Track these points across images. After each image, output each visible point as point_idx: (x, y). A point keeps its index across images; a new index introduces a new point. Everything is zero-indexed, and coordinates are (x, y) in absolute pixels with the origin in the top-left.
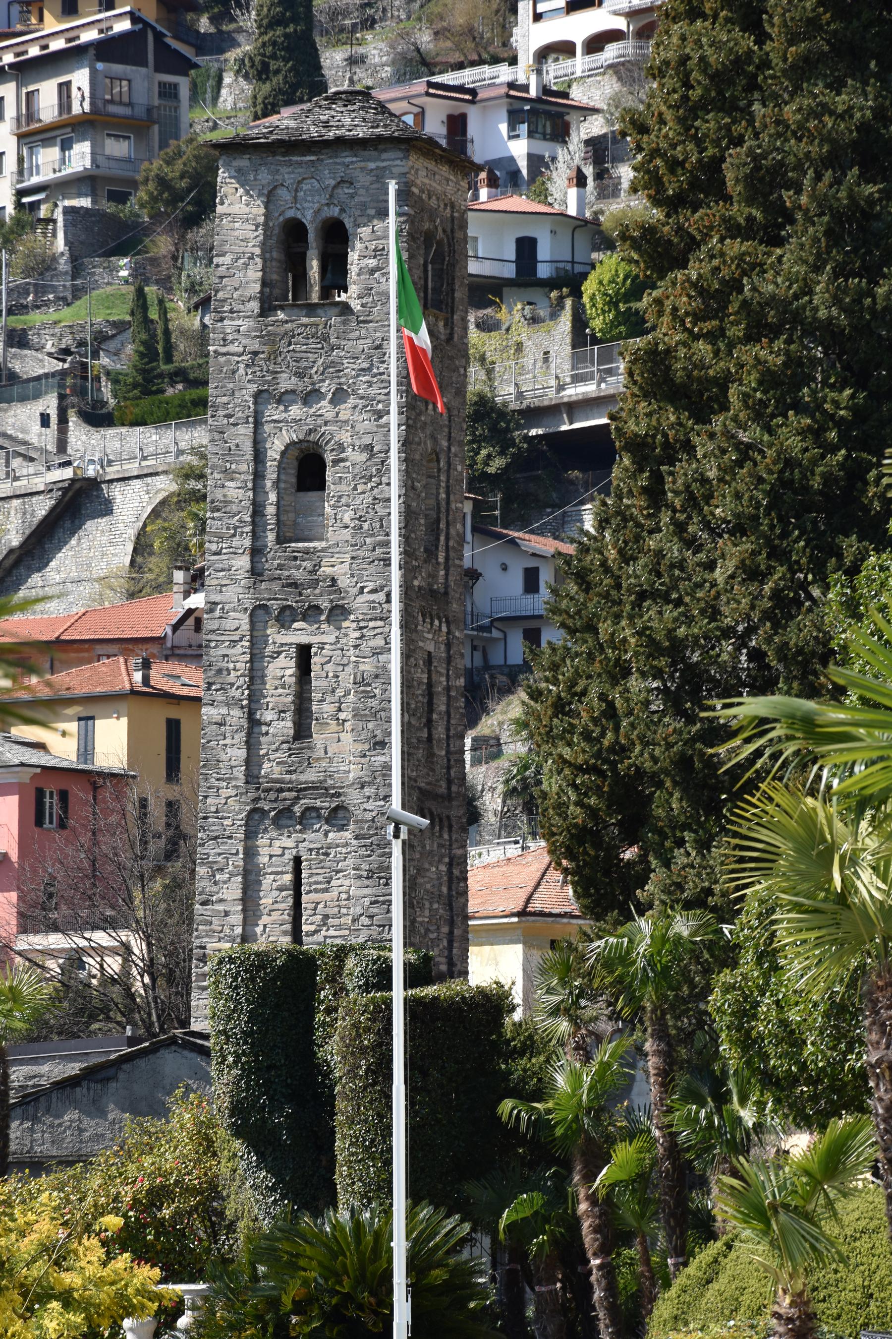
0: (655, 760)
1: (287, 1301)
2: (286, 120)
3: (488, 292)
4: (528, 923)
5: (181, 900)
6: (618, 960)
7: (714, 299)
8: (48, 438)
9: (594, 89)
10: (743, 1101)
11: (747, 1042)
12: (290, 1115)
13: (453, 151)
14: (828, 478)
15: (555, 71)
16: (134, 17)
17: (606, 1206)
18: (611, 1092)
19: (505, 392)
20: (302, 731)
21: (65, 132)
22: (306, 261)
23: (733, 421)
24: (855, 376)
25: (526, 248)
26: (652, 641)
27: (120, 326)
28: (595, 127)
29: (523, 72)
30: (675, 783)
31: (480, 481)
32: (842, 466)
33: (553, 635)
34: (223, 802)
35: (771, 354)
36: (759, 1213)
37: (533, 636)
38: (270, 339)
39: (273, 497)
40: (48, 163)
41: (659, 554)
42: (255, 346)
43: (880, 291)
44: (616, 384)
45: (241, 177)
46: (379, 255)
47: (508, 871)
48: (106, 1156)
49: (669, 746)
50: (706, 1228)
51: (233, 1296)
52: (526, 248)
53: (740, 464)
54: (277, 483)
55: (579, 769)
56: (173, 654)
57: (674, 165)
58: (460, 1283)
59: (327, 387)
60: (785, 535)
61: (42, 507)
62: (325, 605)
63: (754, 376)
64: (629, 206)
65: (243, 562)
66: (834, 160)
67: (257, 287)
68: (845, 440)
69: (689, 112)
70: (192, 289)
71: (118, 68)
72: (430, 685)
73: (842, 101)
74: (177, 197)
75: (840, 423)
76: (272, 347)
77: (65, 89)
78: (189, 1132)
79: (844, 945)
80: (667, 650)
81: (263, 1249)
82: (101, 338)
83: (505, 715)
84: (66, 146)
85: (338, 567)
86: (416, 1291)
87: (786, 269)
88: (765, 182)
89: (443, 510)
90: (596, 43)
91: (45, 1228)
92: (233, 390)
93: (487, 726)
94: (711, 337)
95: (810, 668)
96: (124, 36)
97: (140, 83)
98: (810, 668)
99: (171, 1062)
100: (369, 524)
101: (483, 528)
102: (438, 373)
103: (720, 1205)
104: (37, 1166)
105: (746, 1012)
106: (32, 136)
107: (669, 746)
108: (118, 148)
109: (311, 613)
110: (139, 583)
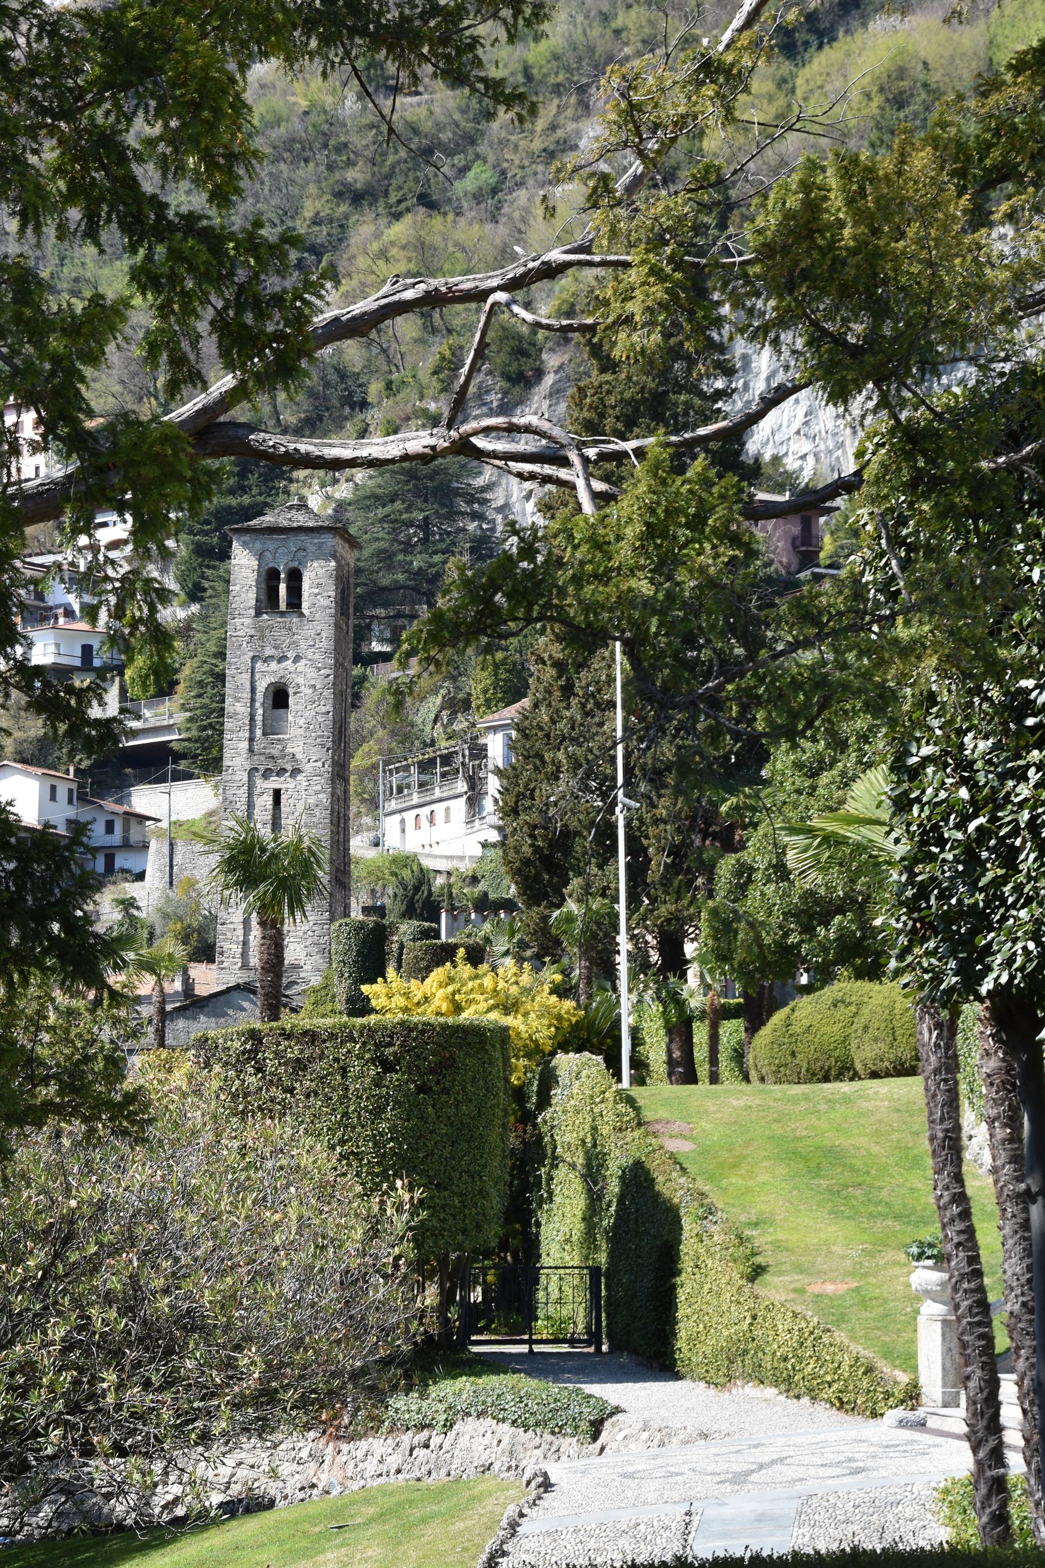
38: (260, 629)
39: (260, 711)
42: (252, 632)
45: (245, 545)
59: (291, 654)
62: (289, 768)
65: (245, 745)
76: (261, 634)
85: (297, 748)
109: (281, 772)
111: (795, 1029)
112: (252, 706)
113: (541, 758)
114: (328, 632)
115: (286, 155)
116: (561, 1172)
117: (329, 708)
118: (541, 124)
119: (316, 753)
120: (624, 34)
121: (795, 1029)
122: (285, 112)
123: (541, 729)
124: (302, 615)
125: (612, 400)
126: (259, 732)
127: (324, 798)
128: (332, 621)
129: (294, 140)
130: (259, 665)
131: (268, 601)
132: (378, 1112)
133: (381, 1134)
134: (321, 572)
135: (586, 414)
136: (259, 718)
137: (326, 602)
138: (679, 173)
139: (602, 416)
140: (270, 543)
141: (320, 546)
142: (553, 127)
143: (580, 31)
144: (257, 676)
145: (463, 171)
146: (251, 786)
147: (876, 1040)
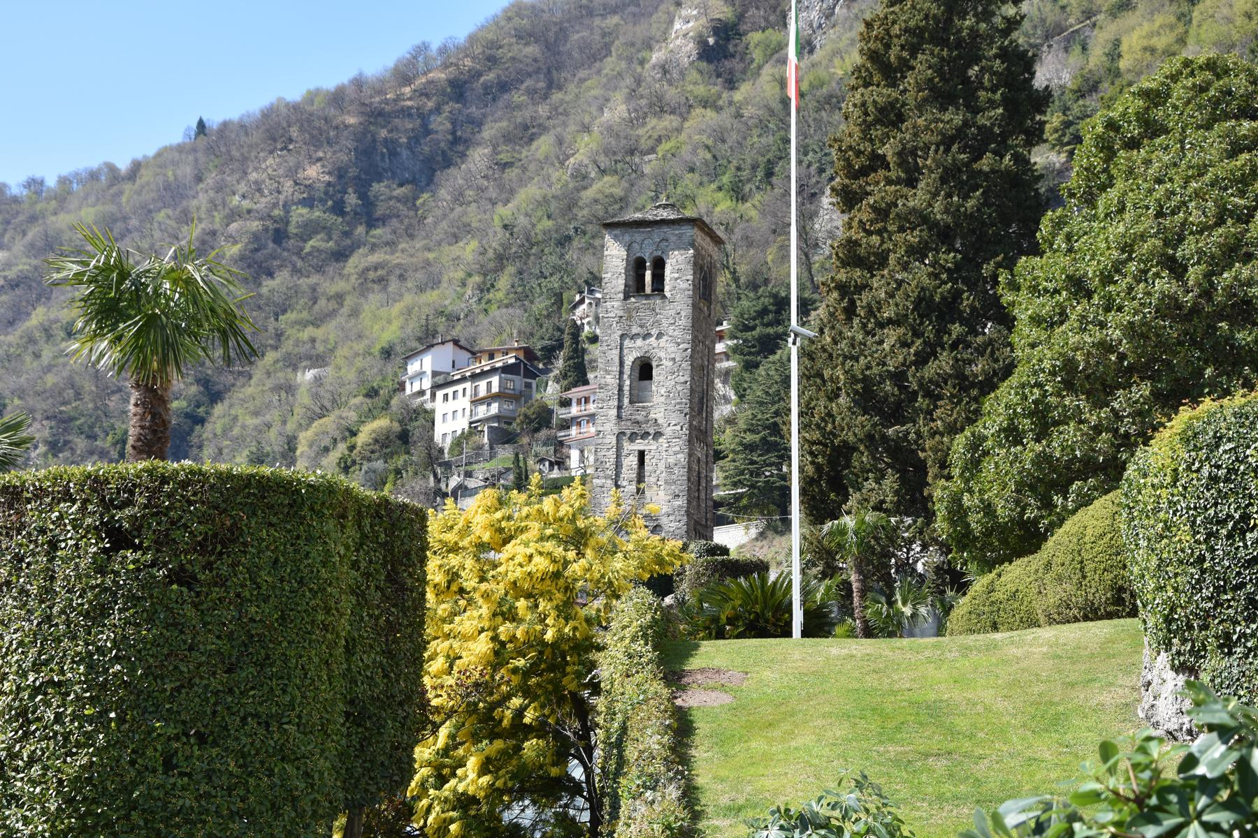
0: (855, 435)
1: (723, 618)
10: (904, 604)
14: (943, 298)
16: (517, 358)
21: (489, 399)
26: (853, 376)
27: (508, 470)
30: (866, 447)
32: (949, 292)
38: (628, 311)
39: (628, 382)
40: (482, 411)
41: (853, 338)
42: (621, 313)
43: (968, 205)
45: (616, 238)
49: (863, 427)
53: (898, 289)
54: (630, 376)
55: (814, 443)
57: (859, 153)
59: (654, 332)
60: (922, 323)
62: (652, 431)
63: (904, 248)
65: (614, 412)
67: (623, 287)
68: (950, 279)
70: (536, 456)
71: (509, 376)
72: (699, 473)
73: (947, 117)
74: (531, 421)
75: (949, 271)
76: (629, 315)
77: (489, 384)
82: (501, 474)
84: (489, 405)
85: (658, 414)
94: (879, 232)
96: (512, 365)
97: (517, 382)
106: (476, 402)
107: (863, 427)
109: (645, 435)
111: (999, 595)
112: (621, 378)
113: (821, 376)
114: (686, 311)
115: (827, 107)
117: (687, 378)
119: (676, 418)
120: (1068, 9)
121: (999, 595)
122: (827, 78)
123: (824, 350)
124: (664, 297)
125: (896, 30)
126: (626, 401)
127: (682, 457)
128: (690, 301)
129: (832, 96)
130: (627, 343)
131: (635, 287)
132: (98, 614)
133: (101, 651)
134: (681, 258)
135: (872, 45)
136: (626, 388)
137: (686, 285)
138: (1100, 86)
139: (888, 46)
140: (638, 235)
141: (680, 237)
143: (1035, 8)
144: (625, 351)
146: (619, 448)
147: (1060, 579)
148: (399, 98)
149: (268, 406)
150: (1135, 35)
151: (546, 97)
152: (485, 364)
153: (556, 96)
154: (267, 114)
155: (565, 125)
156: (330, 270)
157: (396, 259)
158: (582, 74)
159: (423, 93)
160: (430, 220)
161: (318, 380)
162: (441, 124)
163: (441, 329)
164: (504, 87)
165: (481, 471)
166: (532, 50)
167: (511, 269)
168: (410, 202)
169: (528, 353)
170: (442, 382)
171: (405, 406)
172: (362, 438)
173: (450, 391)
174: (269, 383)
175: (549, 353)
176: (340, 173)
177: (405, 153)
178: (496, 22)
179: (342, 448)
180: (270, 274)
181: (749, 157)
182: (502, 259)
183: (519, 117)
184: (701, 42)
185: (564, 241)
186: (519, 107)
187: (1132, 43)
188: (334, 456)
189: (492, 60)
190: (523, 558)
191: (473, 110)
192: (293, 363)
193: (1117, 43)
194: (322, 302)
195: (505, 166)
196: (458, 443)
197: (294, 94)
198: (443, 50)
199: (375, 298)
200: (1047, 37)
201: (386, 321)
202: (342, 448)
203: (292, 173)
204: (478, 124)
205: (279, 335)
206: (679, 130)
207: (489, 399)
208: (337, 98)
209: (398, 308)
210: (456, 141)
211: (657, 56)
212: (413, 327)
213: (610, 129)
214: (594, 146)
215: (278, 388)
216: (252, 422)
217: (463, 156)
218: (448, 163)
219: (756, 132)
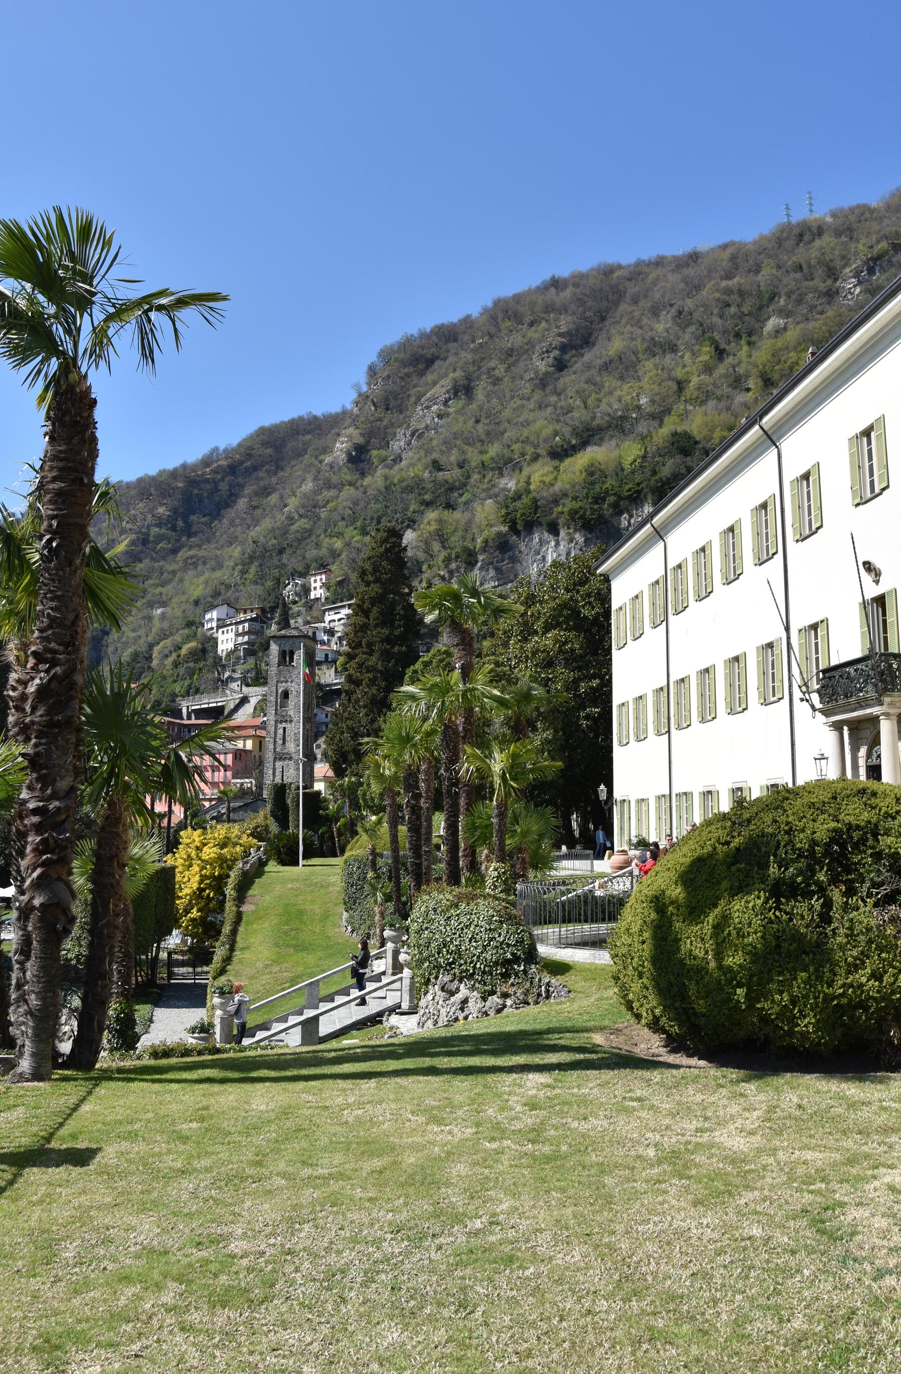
2: (283, 632)
3: (320, 663)
4: (325, 779)
5: (261, 774)
6: (341, 785)
7: (360, 665)
8: (238, 689)
9: (339, 628)
11: (365, 800)
12: (281, 813)
13: (314, 638)
15: (332, 624)
17: (339, 830)
18: (340, 809)
19: (323, 681)
20: (284, 743)
21: (243, 634)
22: (286, 657)
23: (364, 687)
24: (385, 680)
25: (327, 655)
28: (339, 634)
29: (326, 625)
31: (317, 697)
33: (330, 726)
34: (269, 756)
35: (370, 675)
36: (366, 831)
37: (327, 726)
40: (240, 640)
44: (342, 680)
46: (300, 656)
47: (322, 769)
48: (248, 820)
50: (357, 833)
51: (271, 845)
52: (327, 655)
56: (261, 728)
58: (312, 843)
61: (237, 701)
64: (345, 648)
66: (382, 641)
69: (356, 632)
76: (280, 673)
78: (263, 816)
79: (382, 783)
80: (351, 729)
81: (276, 836)
83: (321, 741)
85: (291, 713)
86: (304, 844)
87: (373, 660)
88: (370, 645)
89: (581, 1056)
90: (339, 620)
91: (236, 832)
92: (272, 681)
93: (318, 742)
95: (377, 732)
97: (257, 626)
98: (377, 732)
99: (259, 803)
100: (297, 706)
101: (318, 706)
102: (309, 679)
103: (360, 830)
104: (235, 821)
105: (364, 794)
106: (238, 635)
108: (253, 637)
109: (286, 721)
110: (255, 715)
116: (690, 781)
118: (486, 480)
142: (490, 481)
145: (461, 495)
148: (204, 474)
149: (140, 626)
150: (537, 475)
151: (276, 473)
152: (242, 616)
153: (281, 474)
154: (140, 480)
155: (284, 489)
156: (169, 558)
157: (202, 553)
158: (293, 463)
159: (215, 471)
160: (218, 534)
161: (163, 614)
162: (224, 486)
163: (223, 591)
164: (255, 469)
165: (240, 669)
166: (269, 451)
167: (256, 564)
168: (209, 525)
169: (263, 610)
170: (222, 624)
171: (204, 635)
172: (184, 651)
173: (225, 629)
174: (140, 615)
175: (273, 609)
176: (174, 510)
177: (206, 501)
178: (251, 436)
179: (174, 655)
180: (141, 561)
181: (369, 513)
182: (252, 558)
183: (262, 483)
184: (349, 454)
185: (281, 551)
186: (262, 479)
187: (536, 479)
188: (170, 660)
189: (250, 456)
190: (209, 852)
191: (240, 480)
192: (151, 605)
193: (529, 478)
194: (165, 575)
195: (255, 508)
196: (229, 655)
197: (153, 472)
198: (225, 450)
199: (191, 573)
200: (505, 464)
201: (197, 585)
202: (174, 655)
203: (151, 511)
204: (242, 486)
205: (145, 591)
206: (337, 497)
207: (243, 634)
208: (174, 474)
209: (202, 579)
210: (231, 495)
211: (328, 459)
212: (209, 591)
213: (304, 494)
214: (297, 503)
215: (144, 618)
216: (132, 635)
217: (235, 502)
218: (227, 506)
219: (373, 502)
